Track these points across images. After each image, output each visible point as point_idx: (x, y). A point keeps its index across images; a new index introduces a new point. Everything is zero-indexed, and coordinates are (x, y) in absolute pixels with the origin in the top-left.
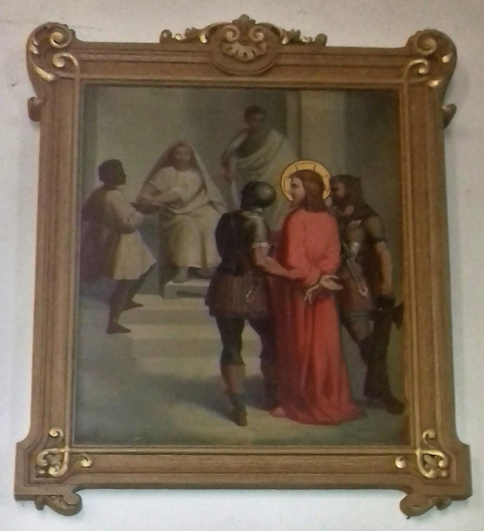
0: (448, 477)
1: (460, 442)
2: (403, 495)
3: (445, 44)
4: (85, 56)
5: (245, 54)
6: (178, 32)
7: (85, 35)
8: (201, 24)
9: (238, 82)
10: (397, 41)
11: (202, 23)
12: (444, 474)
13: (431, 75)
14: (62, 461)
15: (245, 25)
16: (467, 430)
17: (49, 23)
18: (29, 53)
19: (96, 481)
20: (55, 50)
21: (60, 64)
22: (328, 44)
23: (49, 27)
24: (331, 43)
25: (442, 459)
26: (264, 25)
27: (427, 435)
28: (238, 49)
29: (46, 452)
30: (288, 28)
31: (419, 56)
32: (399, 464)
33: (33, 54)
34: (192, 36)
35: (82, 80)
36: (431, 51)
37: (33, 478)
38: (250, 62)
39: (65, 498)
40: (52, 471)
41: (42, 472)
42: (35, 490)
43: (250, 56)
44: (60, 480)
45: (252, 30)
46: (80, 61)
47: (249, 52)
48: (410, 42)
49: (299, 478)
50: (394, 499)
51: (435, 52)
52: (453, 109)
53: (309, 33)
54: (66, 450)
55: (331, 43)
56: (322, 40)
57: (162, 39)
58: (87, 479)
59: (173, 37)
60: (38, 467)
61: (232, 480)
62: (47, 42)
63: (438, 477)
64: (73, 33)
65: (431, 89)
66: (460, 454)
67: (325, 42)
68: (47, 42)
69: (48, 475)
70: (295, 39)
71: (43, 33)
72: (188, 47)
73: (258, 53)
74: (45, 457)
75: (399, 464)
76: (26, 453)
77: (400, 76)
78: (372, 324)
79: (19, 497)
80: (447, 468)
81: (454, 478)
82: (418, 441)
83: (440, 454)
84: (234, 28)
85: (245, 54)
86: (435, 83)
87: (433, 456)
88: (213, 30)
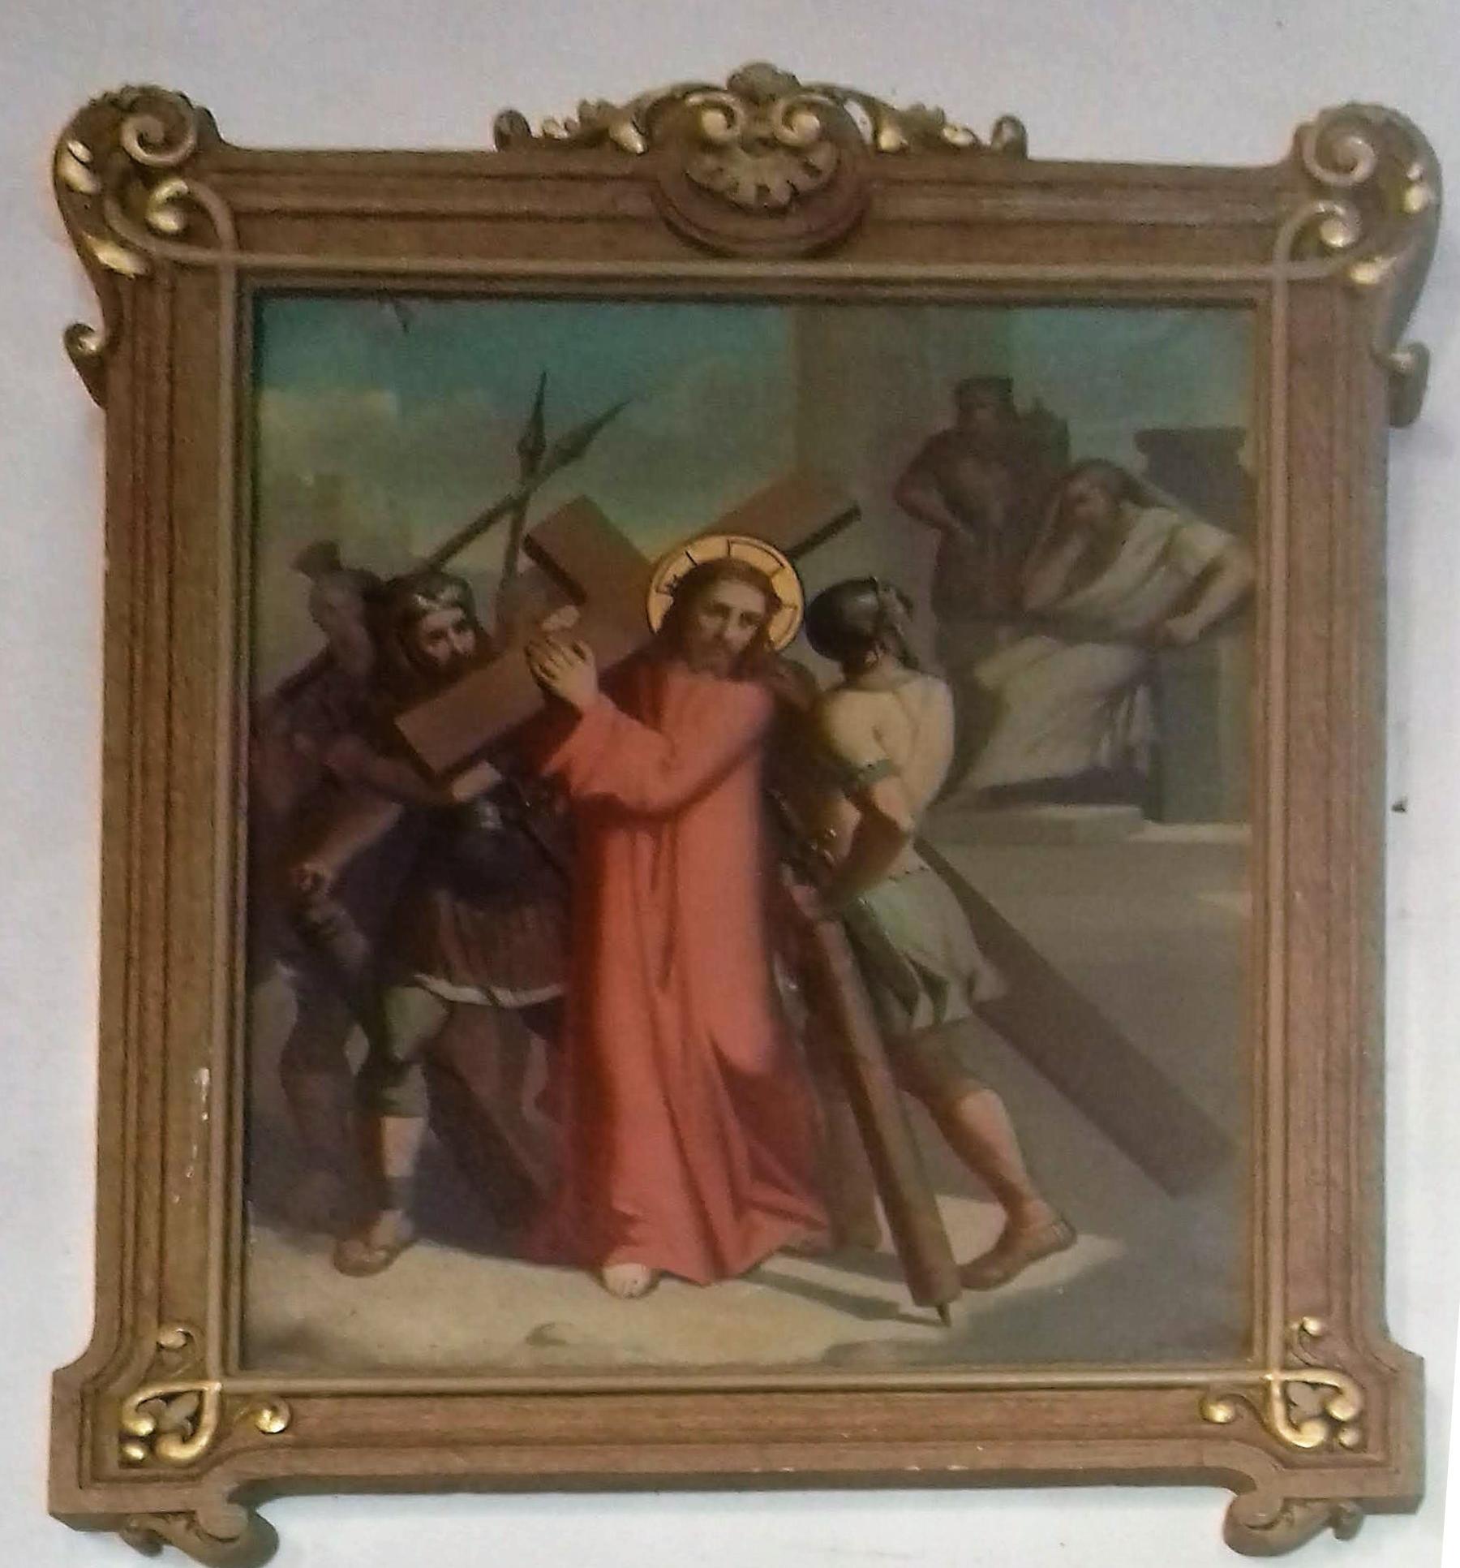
0: (1361, 1446)
3: (1398, 142)
4: (251, 200)
5: (763, 190)
6: (551, 110)
7: (243, 129)
9: (753, 280)
10: (1264, 147)
11: (625, 83)
12: (1348, 1438)
13: (1361, 251)
14: (195, 1418)
15: (755, 90)
16: (1410, 1324)
19: (677, 1467)
20: (149, 177)
21: (168, 222)
23: (128, 98)
24: (1037, 150)
28: (747, 175)
31: (1320, 190)
35: (241, 273)
36: (1362, 171)
37: (112, 1466)
38: (780, 212)
39: (201, 1519)
40: (178, 1452)
41: (136, 1453)
42: (96, 1501)
43: (780, 194)
44: (193, 1472)
45: (781, 105)
46: (237, 216)
47: (771, 177)
49: (788, 1460)
50: (1210, 1508)
51: (1365, 163)
52: (1422, 356)
53: (970, 118)
56: (1012, 141)
57: (501, 138)
58: (276, 1467)
59: (536, 131)
60: (129, 1437)
61: (1118, 1456)
62: (132, 157)
63: (1327, 1447)
66: (1391, 1382)
68: (132, 157)
70: (925, 132)
71: (99, 123)
73: (804, 182)
76: (84, 1403)
77: (1266, 257)
79: (78, 1521)
82: (1275, 1343)
84: (726, 98)
85: (763, 190)
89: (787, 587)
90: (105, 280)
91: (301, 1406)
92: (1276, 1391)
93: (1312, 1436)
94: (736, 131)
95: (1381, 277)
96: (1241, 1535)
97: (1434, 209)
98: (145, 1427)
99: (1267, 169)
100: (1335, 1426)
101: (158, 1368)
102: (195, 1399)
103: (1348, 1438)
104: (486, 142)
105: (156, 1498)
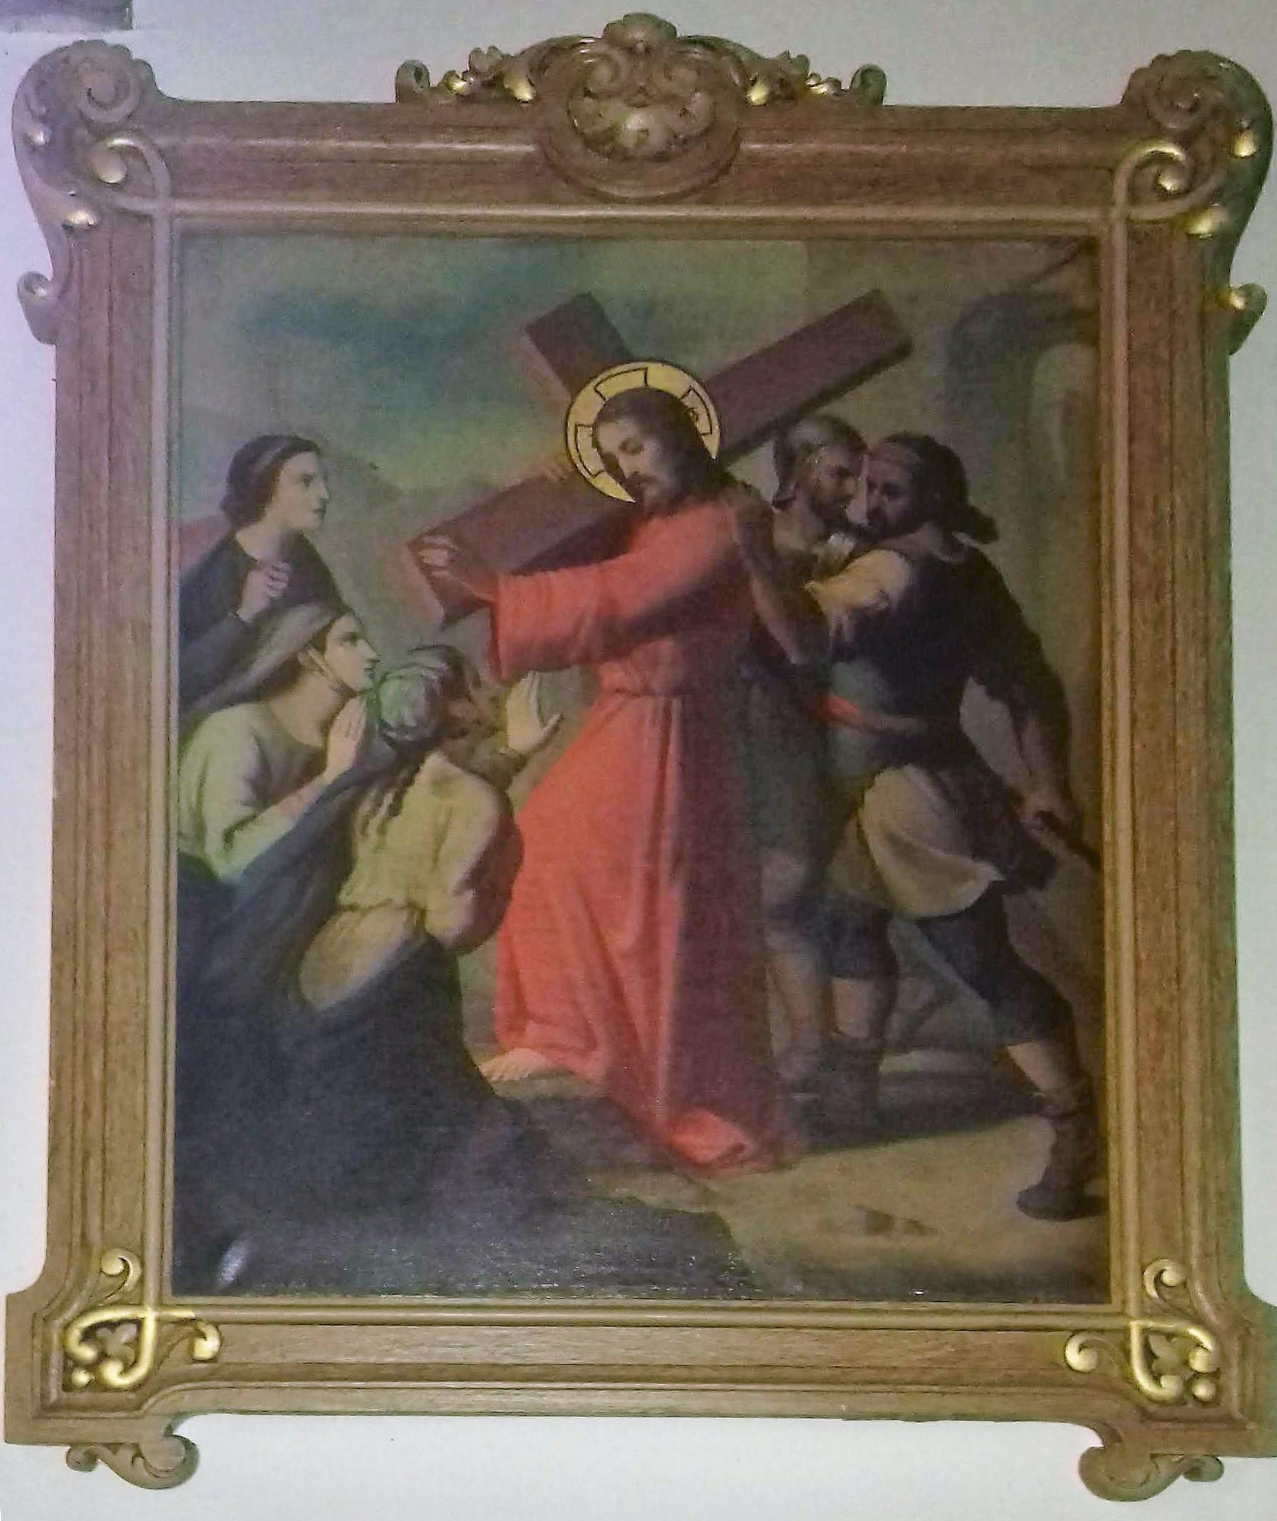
1: (47, 1261)
2: (1094, 1441)
6: (446, 59)
8: (516, 40)
18: (24, 144)
24: (902, 92)
25: (1158, 1280)
27: (1199, 1345)
30: (769, 51)
34: (491, 80)
35: (173, 216)
41: (82, 1378)
54: (150, 1316)
55: (902, 92)
57: (402, 93)
60: (70, 1363)
65: (1193, 238)
69: (98, 1385)
70: (789, 81)
72: (481, 114)
73: (679, 125)
74: (89, 1335)
81: (1233, 1402)
86: (1204, 226)
88: (551, 58)
93: (1169, 1387)
96: (1100, 1475)
97: (1260, 164)
101: (117, 1293)
104: (388, 95)
105: (96, 1429)
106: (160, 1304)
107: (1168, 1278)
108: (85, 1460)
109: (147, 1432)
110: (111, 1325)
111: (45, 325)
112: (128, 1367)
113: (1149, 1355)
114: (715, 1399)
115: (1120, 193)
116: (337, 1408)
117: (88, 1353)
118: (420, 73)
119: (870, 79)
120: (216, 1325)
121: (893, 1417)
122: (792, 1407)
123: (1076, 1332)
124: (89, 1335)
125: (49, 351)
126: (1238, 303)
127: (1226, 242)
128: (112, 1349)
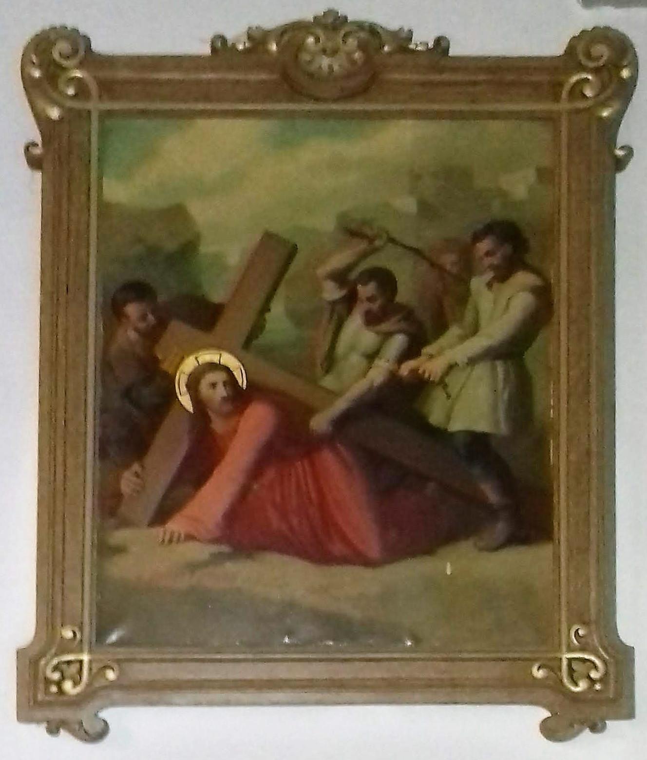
3: (621, 49)
6: (235, 32)
15: (333, 23)
16: (627, 629)
17: (540, 731)
18: (26, 79)
22: (452, 53)
24: (454, 51)
26: (360, 26)
29: (55, 661)
31: (583, 68)
32: (539, 674)
33: (32, 78)
34: (258, 39)
37: (40, 697)
44: (78, 702)
48: (571, 49)
56: (441, 45)
57: (214, 49)
60: (48, 682)
62: (53, 61)
64: (87, 40)
65: (601, 119)
66: (621, 659)
67: (446, 50)
68: (53, 61)
70: (402, 40)
74: (56, 668)
75: (539, 674)
76: (29, 663)
78: (602, 65)
80: (603, 680)
83: (598, 662)
87: (585, 661)
89: (228, 360)
90: (41, 120)
91: (126, 666)
92: (565, 663)
93: (582, 686)
94: (320, 45)
95: (609, 114)
96: (551, 731)
97: (634, 79)
98: (56, 676)
99: (552, 58)
100: (593, 681)
101: (65, 647)
102: (78, 665)
103: (598, 687)
104: (206, 50)
105: (58, 714)
106: (90, 652)
107: (581, 632)
108: (53, 729)
109: (84, 715)
110: (69, 663)
111: (34, 163)
112: (76, 684)
113: (571, 671)
114: (327, 696)
115: (564, 94)
116: (38, 611)
117: (56, 676)
118: (223, 39)
119: (441, 45)
120: (119, 661)
121: (446, 703)
122: (467, 699)
123: (535, 660)
124: (56, 668)
125: (38, 175)
126: (620, 153)
127: (616, 121)
128: (67, 674)
